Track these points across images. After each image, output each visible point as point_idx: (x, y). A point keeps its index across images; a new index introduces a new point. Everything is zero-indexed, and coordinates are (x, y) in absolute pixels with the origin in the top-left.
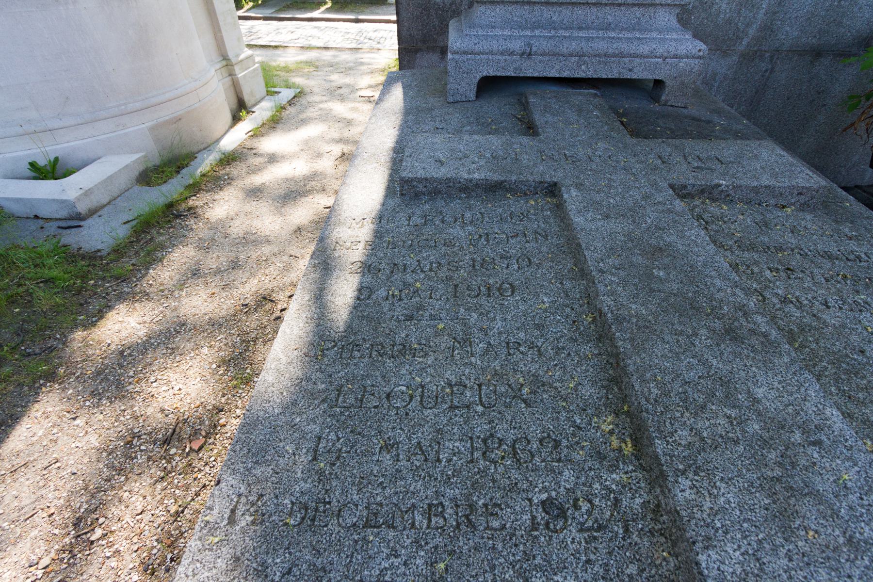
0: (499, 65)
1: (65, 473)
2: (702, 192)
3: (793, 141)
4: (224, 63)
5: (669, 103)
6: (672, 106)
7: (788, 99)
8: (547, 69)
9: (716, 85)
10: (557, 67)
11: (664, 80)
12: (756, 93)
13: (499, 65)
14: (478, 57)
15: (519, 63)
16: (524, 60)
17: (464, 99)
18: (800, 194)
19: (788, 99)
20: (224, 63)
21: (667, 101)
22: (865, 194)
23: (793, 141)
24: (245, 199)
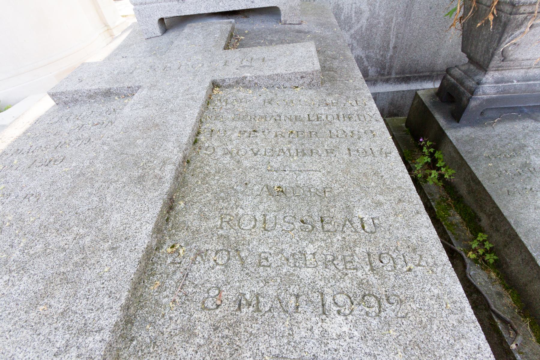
0: (166, 9)
1: (43, 303)
2: (237, 83)
3: (440, 38)
4: (106, 28)
5: (288, 22)
6: (290, 24)
7: (431, 8)
8: (198, 8)
9: (378, 5)
10: (203, 6)
11: (278, 6)
12: (407, 7)
13: (166, 9)
14: (151, 6)
15: (178, 6)
16: (180, 3)
17: (154, 35)
18: (302, 77)
19: (431, 8)
20: (106, 28)
21: (285, 21)
22: (460, 71)
23: (440, 38)
24: (458, 122)
